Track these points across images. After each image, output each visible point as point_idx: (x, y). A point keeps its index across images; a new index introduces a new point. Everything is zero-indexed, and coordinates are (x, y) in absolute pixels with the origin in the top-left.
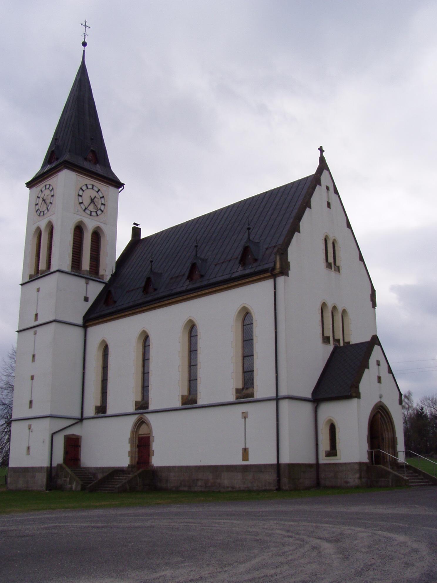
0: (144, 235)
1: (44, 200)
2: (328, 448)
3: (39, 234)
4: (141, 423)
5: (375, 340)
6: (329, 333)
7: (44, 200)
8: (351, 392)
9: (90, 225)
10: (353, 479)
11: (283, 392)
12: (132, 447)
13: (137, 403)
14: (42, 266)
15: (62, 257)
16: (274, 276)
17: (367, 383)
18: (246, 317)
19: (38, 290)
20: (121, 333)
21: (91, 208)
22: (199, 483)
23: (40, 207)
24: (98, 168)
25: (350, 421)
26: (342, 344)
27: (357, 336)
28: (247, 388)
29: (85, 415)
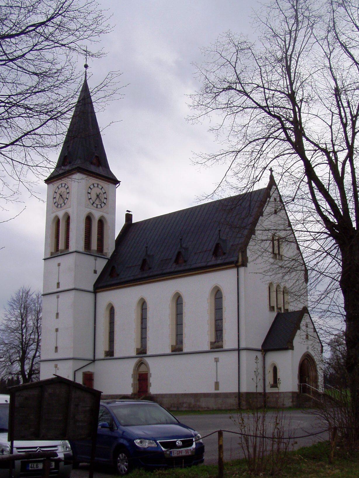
0: (134, 221)
1: (61, 196)
2: (272, 383)
3: (57, 222)
4: (141, 364)
5: (305, 310)
6: (274, 304)
7: (61, 196)
8: (288, 346)
9: (97, 215)
10: (288, 403)
11: (243, 345)
12: (134, 380)
13: (137, 349)
14: (61, 246)
15: (77, 240)
16: (238, 267)
17: (298, 340)
18: (217, 295)
19: (59, 265)
20: (125, 300)
21: (97, 202)
22: (185, 405)
23: (58, 201)
24: (100, 170)
25: (287, 364)
26: (283, 312)
27: (294, 307)
28: (218, 342)
29: (97, 358)
